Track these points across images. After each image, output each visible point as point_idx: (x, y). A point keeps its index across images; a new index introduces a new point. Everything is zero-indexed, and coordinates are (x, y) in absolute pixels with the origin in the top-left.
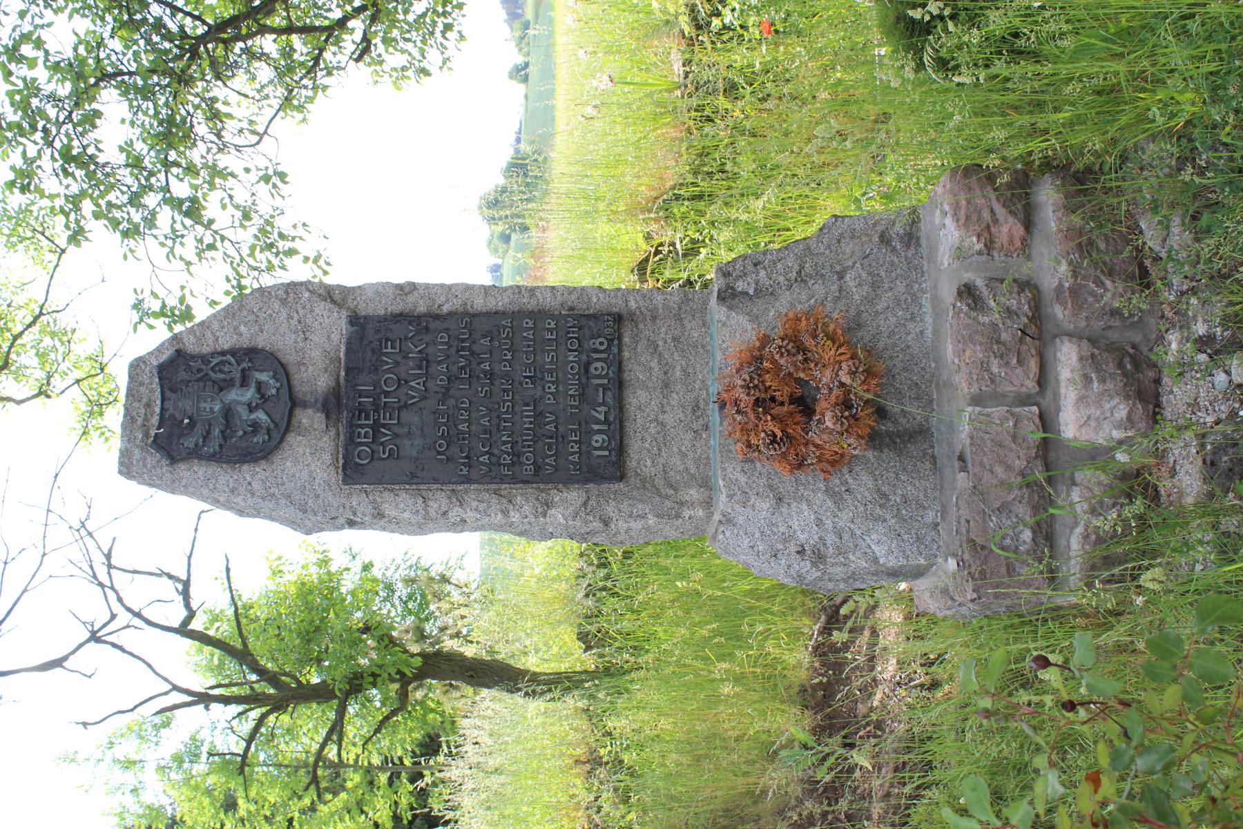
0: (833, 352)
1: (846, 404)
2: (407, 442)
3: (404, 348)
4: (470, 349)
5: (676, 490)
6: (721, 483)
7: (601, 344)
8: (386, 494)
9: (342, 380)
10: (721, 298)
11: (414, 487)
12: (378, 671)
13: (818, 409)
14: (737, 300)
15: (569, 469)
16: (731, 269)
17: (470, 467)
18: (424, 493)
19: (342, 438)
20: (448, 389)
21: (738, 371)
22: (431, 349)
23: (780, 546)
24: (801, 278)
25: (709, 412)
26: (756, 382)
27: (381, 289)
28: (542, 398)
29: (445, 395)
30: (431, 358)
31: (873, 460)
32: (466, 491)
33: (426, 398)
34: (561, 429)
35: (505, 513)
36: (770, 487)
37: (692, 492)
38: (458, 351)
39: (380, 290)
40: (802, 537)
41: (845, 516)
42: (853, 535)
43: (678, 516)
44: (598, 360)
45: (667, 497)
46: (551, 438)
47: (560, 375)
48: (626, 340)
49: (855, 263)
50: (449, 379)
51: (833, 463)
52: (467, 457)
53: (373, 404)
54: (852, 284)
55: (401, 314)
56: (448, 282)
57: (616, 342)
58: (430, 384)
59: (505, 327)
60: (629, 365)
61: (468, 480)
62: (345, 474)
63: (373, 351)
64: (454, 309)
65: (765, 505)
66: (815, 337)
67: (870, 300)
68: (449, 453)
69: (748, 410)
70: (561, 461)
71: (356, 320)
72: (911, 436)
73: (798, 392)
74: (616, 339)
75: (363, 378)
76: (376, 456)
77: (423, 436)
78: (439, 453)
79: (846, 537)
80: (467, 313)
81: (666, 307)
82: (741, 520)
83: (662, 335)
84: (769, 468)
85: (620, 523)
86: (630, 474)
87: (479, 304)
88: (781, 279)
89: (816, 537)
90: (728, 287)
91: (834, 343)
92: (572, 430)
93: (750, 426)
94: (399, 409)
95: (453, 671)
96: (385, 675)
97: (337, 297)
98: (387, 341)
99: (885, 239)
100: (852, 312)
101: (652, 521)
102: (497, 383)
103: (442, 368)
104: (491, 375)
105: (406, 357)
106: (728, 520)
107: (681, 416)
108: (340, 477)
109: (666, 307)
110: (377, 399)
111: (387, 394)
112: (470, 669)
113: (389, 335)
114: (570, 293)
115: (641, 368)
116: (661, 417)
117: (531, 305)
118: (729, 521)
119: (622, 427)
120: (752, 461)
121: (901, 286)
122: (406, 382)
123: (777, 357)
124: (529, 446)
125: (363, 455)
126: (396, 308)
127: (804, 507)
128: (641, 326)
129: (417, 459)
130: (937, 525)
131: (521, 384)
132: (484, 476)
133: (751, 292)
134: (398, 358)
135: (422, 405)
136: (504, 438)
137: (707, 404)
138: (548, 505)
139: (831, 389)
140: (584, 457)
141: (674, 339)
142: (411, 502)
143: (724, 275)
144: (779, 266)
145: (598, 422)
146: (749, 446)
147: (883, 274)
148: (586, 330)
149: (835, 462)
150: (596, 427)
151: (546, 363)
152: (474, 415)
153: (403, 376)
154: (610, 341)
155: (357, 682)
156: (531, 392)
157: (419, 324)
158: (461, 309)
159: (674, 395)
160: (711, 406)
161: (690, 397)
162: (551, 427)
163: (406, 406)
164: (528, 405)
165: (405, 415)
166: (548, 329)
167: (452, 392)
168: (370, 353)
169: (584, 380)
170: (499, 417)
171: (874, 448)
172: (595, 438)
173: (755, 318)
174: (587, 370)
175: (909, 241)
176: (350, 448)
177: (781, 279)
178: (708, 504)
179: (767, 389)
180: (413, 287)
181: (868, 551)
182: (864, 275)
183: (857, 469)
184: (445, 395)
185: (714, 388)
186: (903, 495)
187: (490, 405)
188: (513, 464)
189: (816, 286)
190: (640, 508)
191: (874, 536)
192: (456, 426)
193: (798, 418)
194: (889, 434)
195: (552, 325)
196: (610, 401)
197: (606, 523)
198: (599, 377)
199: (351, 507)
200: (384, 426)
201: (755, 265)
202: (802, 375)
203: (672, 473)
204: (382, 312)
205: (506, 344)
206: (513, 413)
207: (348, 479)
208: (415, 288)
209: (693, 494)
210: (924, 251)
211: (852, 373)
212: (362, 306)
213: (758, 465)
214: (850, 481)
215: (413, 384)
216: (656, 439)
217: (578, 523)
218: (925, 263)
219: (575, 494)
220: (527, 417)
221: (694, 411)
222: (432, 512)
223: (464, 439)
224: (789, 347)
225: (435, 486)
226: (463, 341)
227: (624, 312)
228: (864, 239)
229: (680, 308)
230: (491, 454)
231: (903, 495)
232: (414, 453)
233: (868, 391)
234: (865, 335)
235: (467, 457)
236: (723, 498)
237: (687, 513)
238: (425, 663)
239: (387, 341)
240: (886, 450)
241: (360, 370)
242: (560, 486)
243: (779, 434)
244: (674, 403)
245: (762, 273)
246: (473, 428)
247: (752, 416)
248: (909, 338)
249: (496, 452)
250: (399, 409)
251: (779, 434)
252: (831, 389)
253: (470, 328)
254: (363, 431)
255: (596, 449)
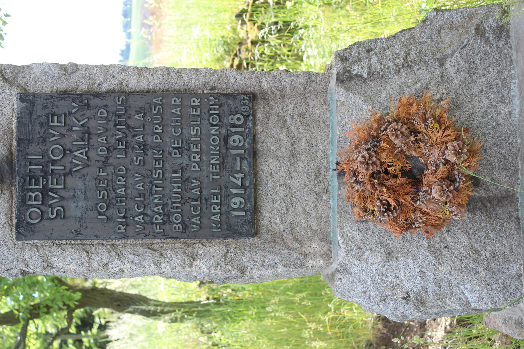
0: (440, 133)
1: (450, 179)
2: (72, 204)
3: (68, 122)
4: (126, 124)
5: (301, 244)
6: (340, 240)
7: (239, 119)
8: (54, 248)
9: (14, 149)
10: (340, 81)
11: (79, 242)
12: (50, 304)
13: (425, 181)
14: (353, 83)
15: (212, 227)
16: (347, 55)
17: (127, 225)
18: (88, 248)
19: (15, 200)
20: (107, 158)
21: (356, 147)
22: (92, 124)
23: (388, 293)
24: (407, 64)
25: (329, 178)
26: (374, 159)
27: (47, 69)
28: (188, 166)
29: (105, 163)
30: (92, 131)
31: (467, 221)
32: (124, 246)
33: (88, 166)
34: (205, 193)
35: (157, 264)
36: (382, 243)
37: (315, 245)
38: (115, 125)
39: (47, 69)
40: (408, 286)
41: (444, 269)
42: (450, 284)
43: (302, 266)
44: (236, 133)
45: (294, 250)
46: (196, 200)
47: (204, 146)
48: (259, 115)
49: (454, 52)
50: (108, 150)
51: (436, 227)
52: (124, 217)
53: (42, 171)
54: (452, 70)
55: (65, 92)
56: (107, 64)
57: (251, 118)
58: (92, 154)
59: (156, 105)
60: (261, 138)
61: (126, 236)
62: (18, 232)
63: (42, 124)
64: (112, 87)
65: (377, 259)
66: (425, 121)
67: (466, 85)
68: (109, 213)
69: (366, 180)
70: (205, 221)
71: (26, 97)
72: (499, 201)
73: (409, 166)
74: (250, 115)
75: (33, 148)
76: (45, 216)
77: (86, 199)
78: (100, 214)
79: (444, 286)
80: (123, 92)
81: (293, 88)
82: (355, 270)
83: (290, 112)
84: (381, 228)
85: (254, 271)
86: (263, 230)
87: (134, 83)
88: (391, 64)
89: (419, 286)
90: (346, 71)
91: (440, 125)
92: (214, 194)
93: (367, 194)
94: (65, 175)
95: (106, 302)
96: (56, 307)
97: (9, 76)
98: (53, 115)
99: (479, 31)
100: (452, 95)
101: (280, 270)
102: (150, 153)
103: (102, 140)
104: (144, 146)
105: (70, 130)
106: (345, 270)
107: (306, 181)
108: (14, 233)
109: (293, 88)
110: (45, 166)
111: (54, 162)
112: (117, 300)
113: (55, 110)
114: (211, 75)
115: (272, 139)
116: (288, 182)
117: (179, 85)
118: (346, 271)
119: (255, 189)
120: (366, 221)
121: (493, 73)
122: (71, 152)
123: (393, 138)
124: (177, 208)
125: (34, 215)
126: (62, 86)
127: (410, 260)
128: (272, 104)
129: (81, 219)
130: (520, 276)
131: (170, 154)
132: (139, 233)
133: (365, 75)
134: (64, 131)
135: (85, 171)
136: (156, 201)
137: (327, 170)
138: (193, 257)
139: (437, 166)
140: (224, 218)
141: (300, 115)
142: (76, 256)
143: (342, 60)
144: (388, 52)
145: (236, 187)
146: (365, 210)
147: (478, 62)
148: (226, 107)
149: (436, 225)
150: (234, 191)
151: (192, 136)
152: (130, 181)
153: (68, 146)
154: (246, 117)
155: (36, 312)
156: (179, 161)
157: (82, 101)
158: (117, 88)
159: (300, 163)
160: (331, 172)
161: (313, 165)
162: (196, 191)
163: (71, 172)
164: (176, 172)
165: (70, 180)
166: (193, 107)
167: (111, 161)
168: (38, 127)
169: (224, 151)
170: (151, 182)
171: (469, 211)
172: (234, 200)
173: (369, 100)
174: (226, 142)
175: (500, 33)
176: (23, 209)
177: (391, 64)
178: (328, 256)
179: (382, 163)
180: (75, 67)
181: (462, 297)
182: (462, 63)
183: (454, 228)
184: (105, 163)
185: (333, 158)
186: (492, 251)
187: (144, 172)
188: (164, 223)
189: (421, 71)
190: (270, 258)
191: (468, 286)
192: (114, 190)
193: (409, 189)
194: (481, 199)
195: (197, 103)
196: (246, 168)
197: (242, 272)
198: (237, 148)
199: (24, 260)
200: (52, 190)
201: (368, 51)
202: (413, 154)
203: (298, 229)
204: (49, 90)
205: (156, 119)
206: (164, 179)
207: (20, 236)
208: (78, 69)
209: (315, 247)
210: (513, 41)
211: (458, 154)
212: (31, 83)
213: (371, 224)
214: (448, 239)
215: (76, 153)
216: (284, 200)
217: (219, 271)
218: (514, 52)
219: (216, 248)
220: (176, 182)
221: (316, 177)
222: (95, 264)
223: (121, 202)
224: (403, 130)
225: (97, 241)
226: (120, 116)
227: (257, 92)
228: (461, 30)
229: (305, 89)
230: (145, 215)
231: (492, 251)
232: (79, 214)
233: (469, 167)
234: (461, 116)
235: (124, 217)
236: (342, 252)
237: (310, 263)
238: (83, 297)
239: (53, 115)
240: (478, 213)
241: (30, 142)
242: (204, 241)
243: (393, 203)
244: (300, 170)
245: (374, 59)
246: (129, 192)
247: (369, 186)
248: (500, 117)
249: (149, 212)
250: (65, 175)
251: (393, 203)
252: (437, 166)
253: (125, 103)
254: (33, 195)
255: (234, 210)
